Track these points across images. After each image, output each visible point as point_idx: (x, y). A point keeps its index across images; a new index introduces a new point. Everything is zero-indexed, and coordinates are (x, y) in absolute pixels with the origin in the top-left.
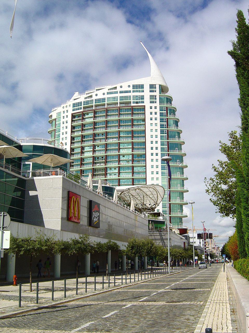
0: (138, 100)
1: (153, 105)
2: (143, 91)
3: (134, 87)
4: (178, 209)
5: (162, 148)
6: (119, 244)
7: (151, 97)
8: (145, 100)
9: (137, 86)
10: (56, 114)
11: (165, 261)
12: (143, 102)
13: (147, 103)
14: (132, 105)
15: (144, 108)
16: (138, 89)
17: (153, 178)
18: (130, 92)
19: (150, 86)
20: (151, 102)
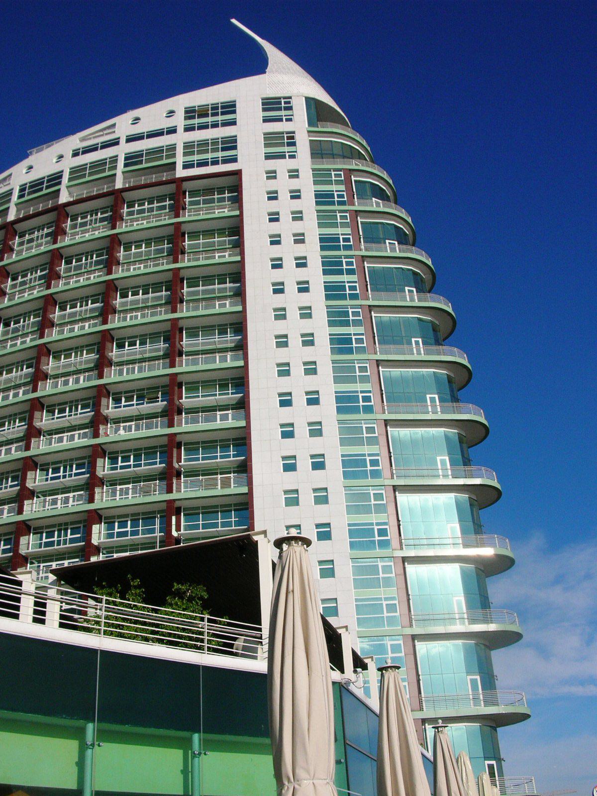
0: (210, 156)
1: (282, 166)
2: (233, 123)
3: (190, 113)
4: (486, 758)
5: (341, 398)
6: (388, 672)
7: (271, 139)
8: (240, 116)
9: (220, 325)
10: (67, 564)
11: (119, 585)
12: (234, 160)
13: (251, 161)
14: (180, 173)
15: (233, 185)
16: (210, 156)
17: (319, 465)
18: (172, 131)
19: (263, 104)
20: (268, 157)
